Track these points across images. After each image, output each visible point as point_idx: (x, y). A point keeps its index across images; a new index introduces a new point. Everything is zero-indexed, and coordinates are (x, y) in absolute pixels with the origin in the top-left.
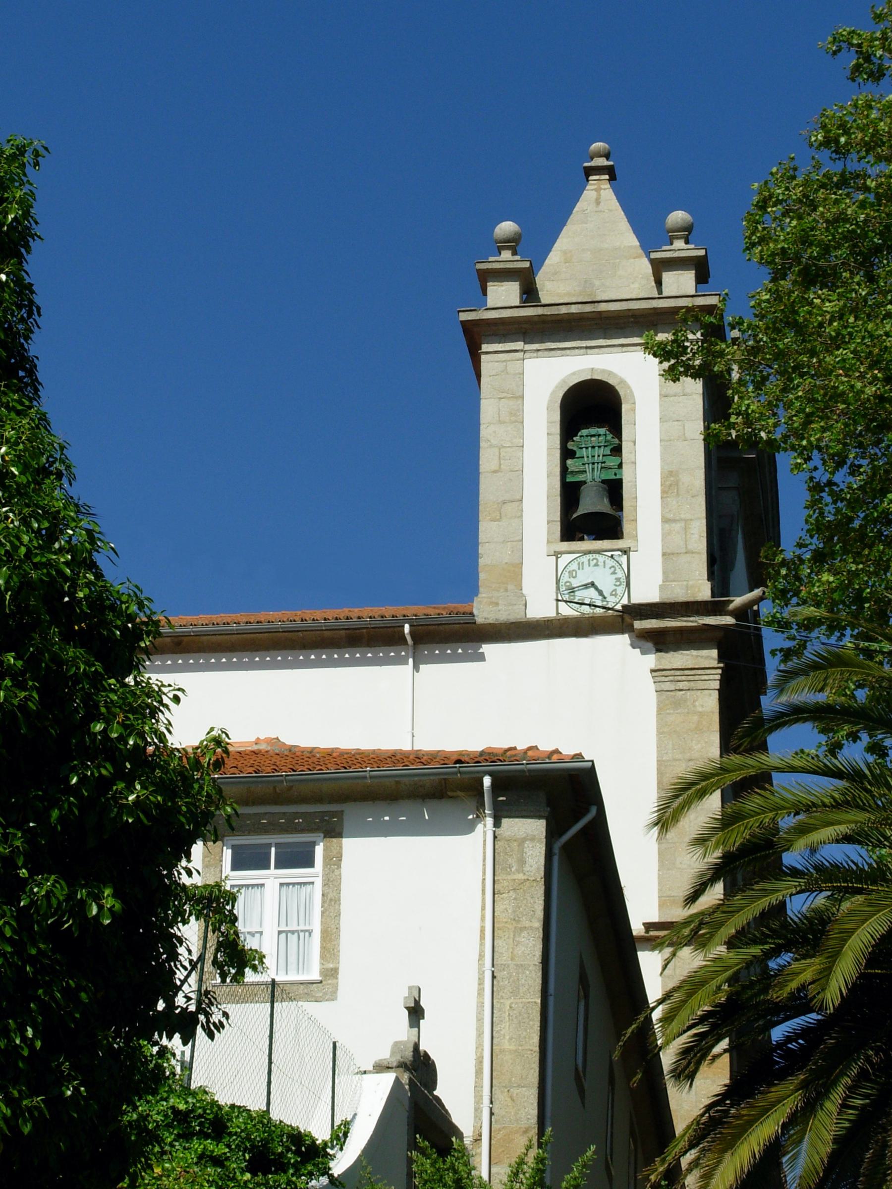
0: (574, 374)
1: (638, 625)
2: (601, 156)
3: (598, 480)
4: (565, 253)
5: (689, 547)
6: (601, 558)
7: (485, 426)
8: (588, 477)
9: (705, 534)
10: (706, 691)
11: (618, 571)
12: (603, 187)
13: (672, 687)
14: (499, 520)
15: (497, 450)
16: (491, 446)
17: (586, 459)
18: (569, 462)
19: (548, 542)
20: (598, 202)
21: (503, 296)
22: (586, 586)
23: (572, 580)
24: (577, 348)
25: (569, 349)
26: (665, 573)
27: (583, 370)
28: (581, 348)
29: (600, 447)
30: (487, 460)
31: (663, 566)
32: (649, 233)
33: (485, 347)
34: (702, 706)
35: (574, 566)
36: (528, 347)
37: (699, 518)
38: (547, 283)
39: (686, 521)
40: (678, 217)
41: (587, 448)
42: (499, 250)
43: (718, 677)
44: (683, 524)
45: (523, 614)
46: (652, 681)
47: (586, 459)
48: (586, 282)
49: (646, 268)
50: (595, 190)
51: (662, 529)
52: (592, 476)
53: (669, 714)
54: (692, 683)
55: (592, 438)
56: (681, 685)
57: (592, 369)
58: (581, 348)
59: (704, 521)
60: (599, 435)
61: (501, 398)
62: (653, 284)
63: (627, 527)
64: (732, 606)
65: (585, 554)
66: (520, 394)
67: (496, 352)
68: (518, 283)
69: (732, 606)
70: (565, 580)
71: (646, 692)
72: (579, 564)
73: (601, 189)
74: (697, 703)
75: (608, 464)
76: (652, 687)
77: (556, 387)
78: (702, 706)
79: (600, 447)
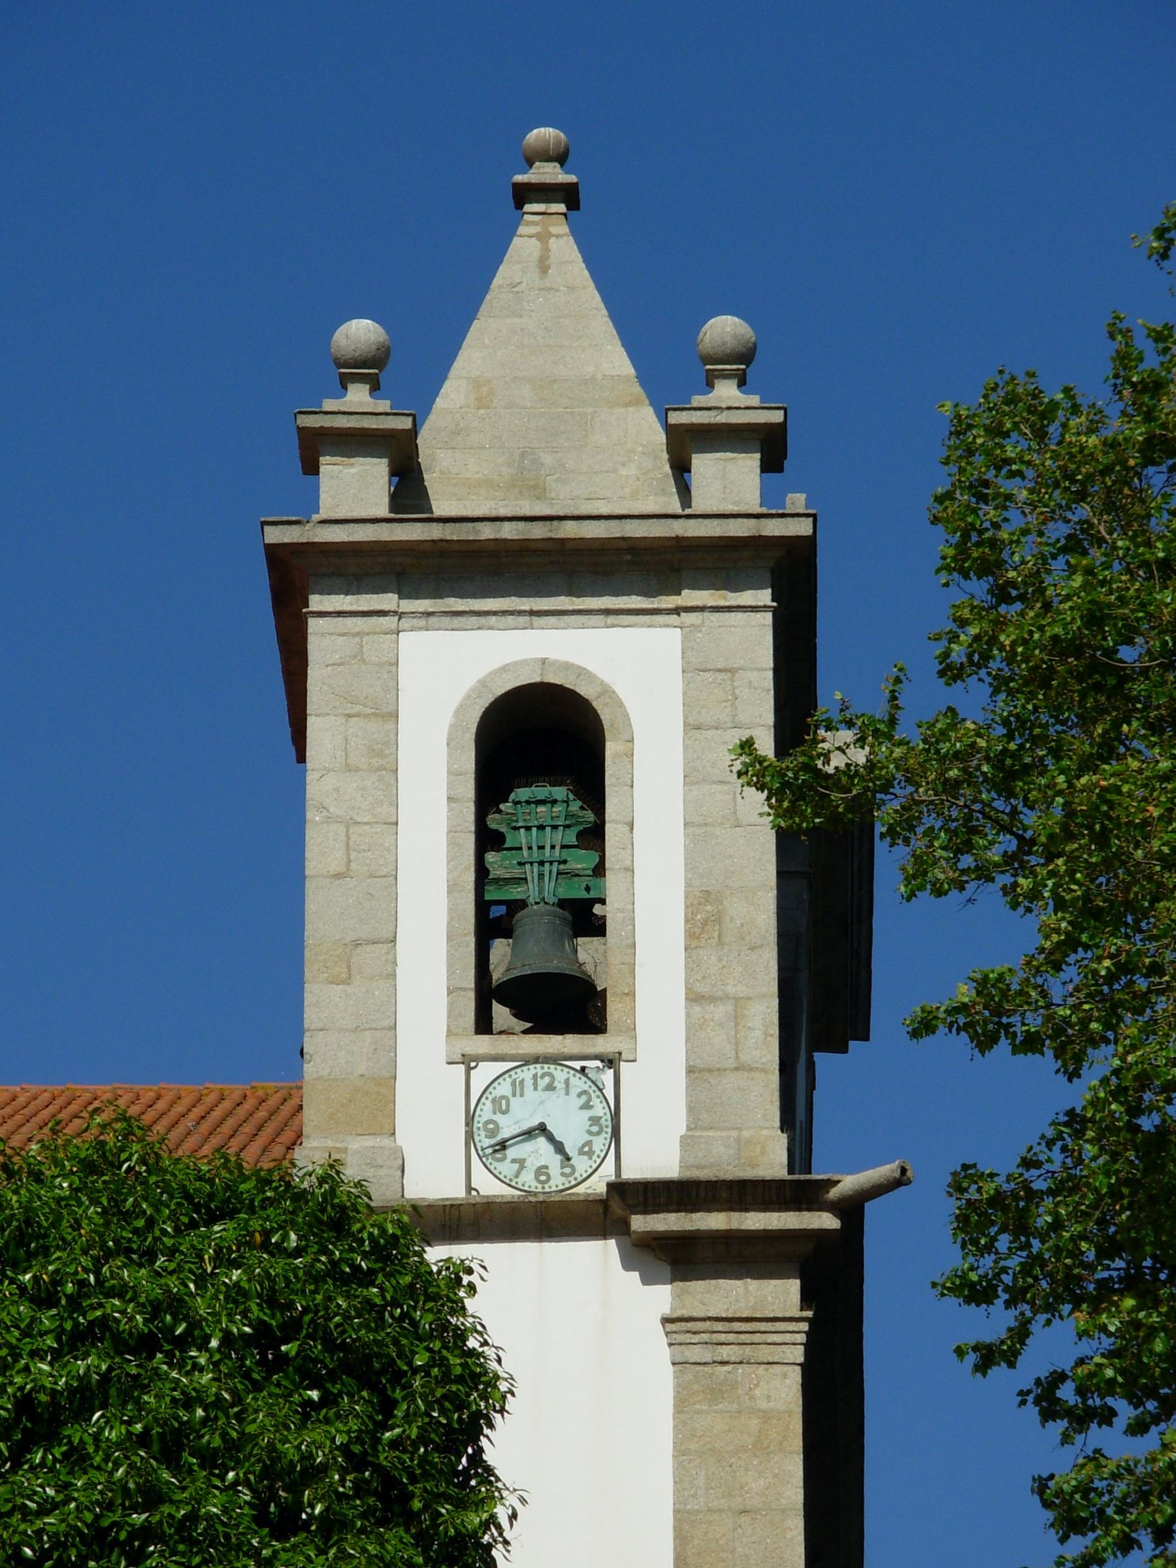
0: (504, 669)
1: (640, 1223)
2: (549, 159)
3: (553, 900)
4: (477, 383)
5: (744, 1057)
6: (560, 1074)
7: (316, 775)
8: (530, 892)
9: (775, 1031)
10: (777, 1369)
11: (596, 1101)
12: (554, 230)
13: (707, 1358)
14: (347, 981)
15: (342, 829)
16: (329, 820)
17: (525, 852)
18: (491, 857)
19: (450, 1033)
20: (543, 267)
21: (353, 491)
22: (529, 1134)
23: (498, 1118)
24: (512, 613)
25: (495, 613)
26: (692, 1110)
27: (524, 663)
28: (520, 613)
29: (555, 827)
30: (322, 849)
31: (689, 1095)
32: (665, 364)
33: (317, 602)
34: (768, 1397)
35: (504, 1088)
36: (407, 605)
37: (764, 996)
38: (440, 454)
39: (737, 999)
40: (724, 329)
41: (528, 828)
42: (344, 382)
43: (802, 1338)
44: (729, 1007)
45: (398, 1187)
46: (665, 1341)
47: (525, 852)
48: (523, 455)
49: (646, 431)
50: (538, 236)
51: (688, 1015)
52: (540, 890)
53: (700, 1412)
54: (748, 1349)
55: (541, 805)
56: (725, 1353)
57: (544, 661)
58: (520, 613)
59: (775, 1003)
60: (554, 802)
61: (349, 716)
62: (667, 468)
63: (614, 1010)
64: (834, 1193)
65: (527, 1063)
66: (391, 708)
67: (339, 614)
68: (385, 461)
69: (834, 1193)
70: (484, 1119)
71: (652, 1367)
72: (513, 1083)
73: (551, 235)
74: (757, 1392)
75: (573, 865)
76: (664, 1354)
77: (468, 697)
78: (768, 1397)
79: (555, 827)
